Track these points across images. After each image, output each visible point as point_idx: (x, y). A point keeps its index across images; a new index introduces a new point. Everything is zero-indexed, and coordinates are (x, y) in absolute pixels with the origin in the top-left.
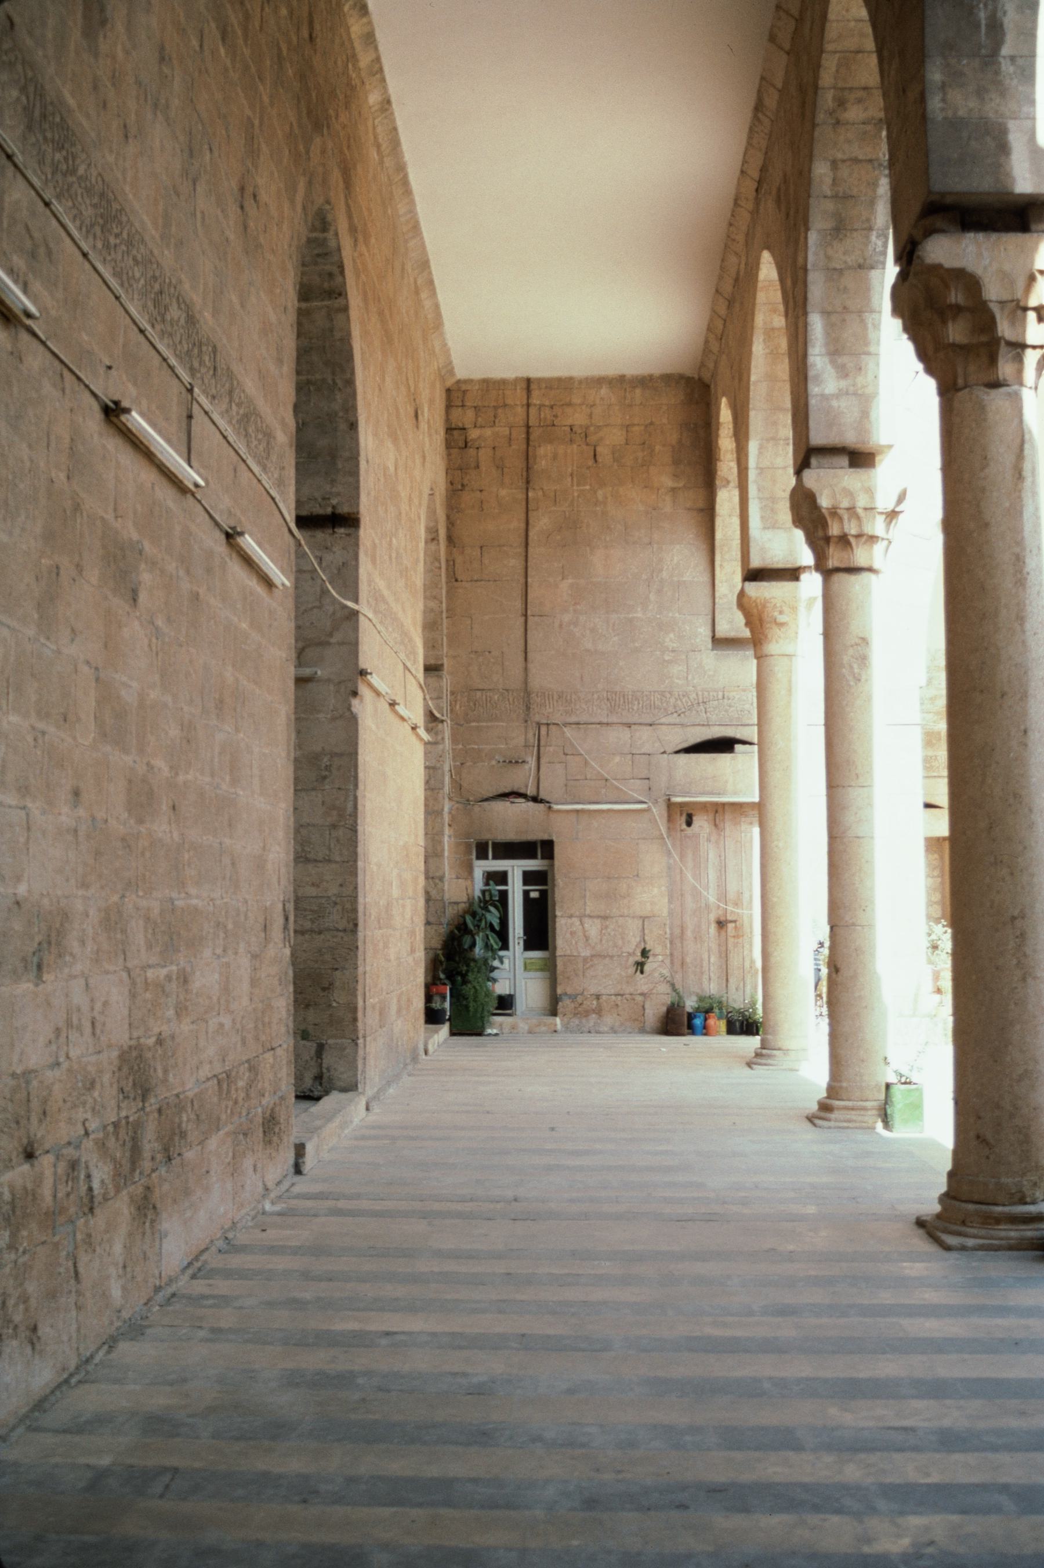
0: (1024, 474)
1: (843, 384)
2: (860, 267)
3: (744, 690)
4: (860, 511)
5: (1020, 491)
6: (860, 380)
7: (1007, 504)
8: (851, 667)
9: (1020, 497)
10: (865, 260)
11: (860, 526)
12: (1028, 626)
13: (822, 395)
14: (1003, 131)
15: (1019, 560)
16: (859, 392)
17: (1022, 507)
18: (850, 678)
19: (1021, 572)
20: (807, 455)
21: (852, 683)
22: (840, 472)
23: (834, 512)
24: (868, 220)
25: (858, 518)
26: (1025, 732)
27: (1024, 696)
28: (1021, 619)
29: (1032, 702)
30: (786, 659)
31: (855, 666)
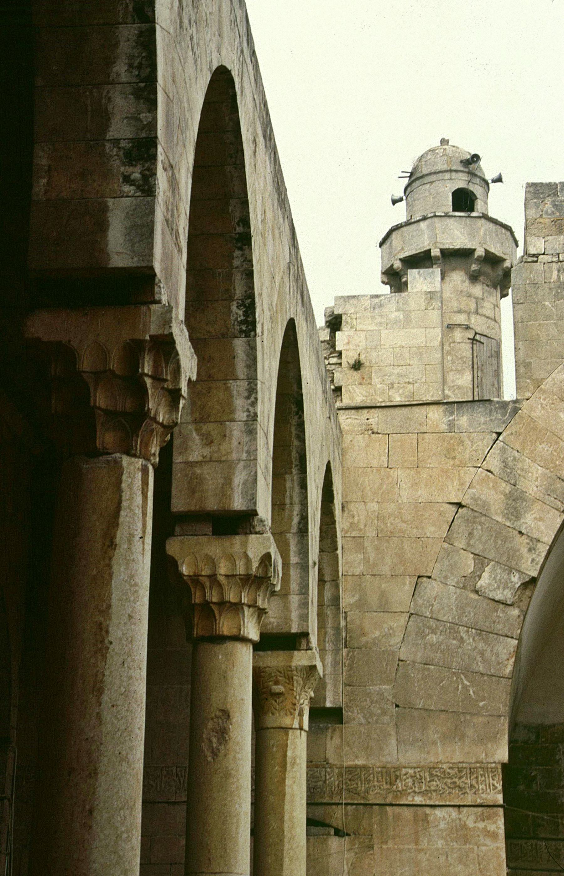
0: (117, 540)
1: (206, 451)
2: (224, 336)
3: (317, 767)
4: (222, 579)
5: (110, 559)
6: (224, 447)
7: (95, 572)
8: (210, 741)
9: (109, 566)
10: (228, 329)
11: (221, 593)
12: (105, 697)
13: (187, 463)
14: (104, 209)
15: (102, 630)
16: (223, 459)
17: (111, 575)
18: (209, 754)
19: (102, 642)
20: (166, 523)
21: (210, 759)
22: (204, 539)
23: (195, 579)
24: (227, 290)
25: (220, 585)
26: (91, 812)
27: (94, 774)
28: (98, 690)
29: (102, 778)
30: (282, 733)
31: (214, 740)
